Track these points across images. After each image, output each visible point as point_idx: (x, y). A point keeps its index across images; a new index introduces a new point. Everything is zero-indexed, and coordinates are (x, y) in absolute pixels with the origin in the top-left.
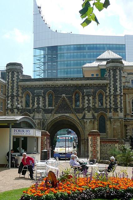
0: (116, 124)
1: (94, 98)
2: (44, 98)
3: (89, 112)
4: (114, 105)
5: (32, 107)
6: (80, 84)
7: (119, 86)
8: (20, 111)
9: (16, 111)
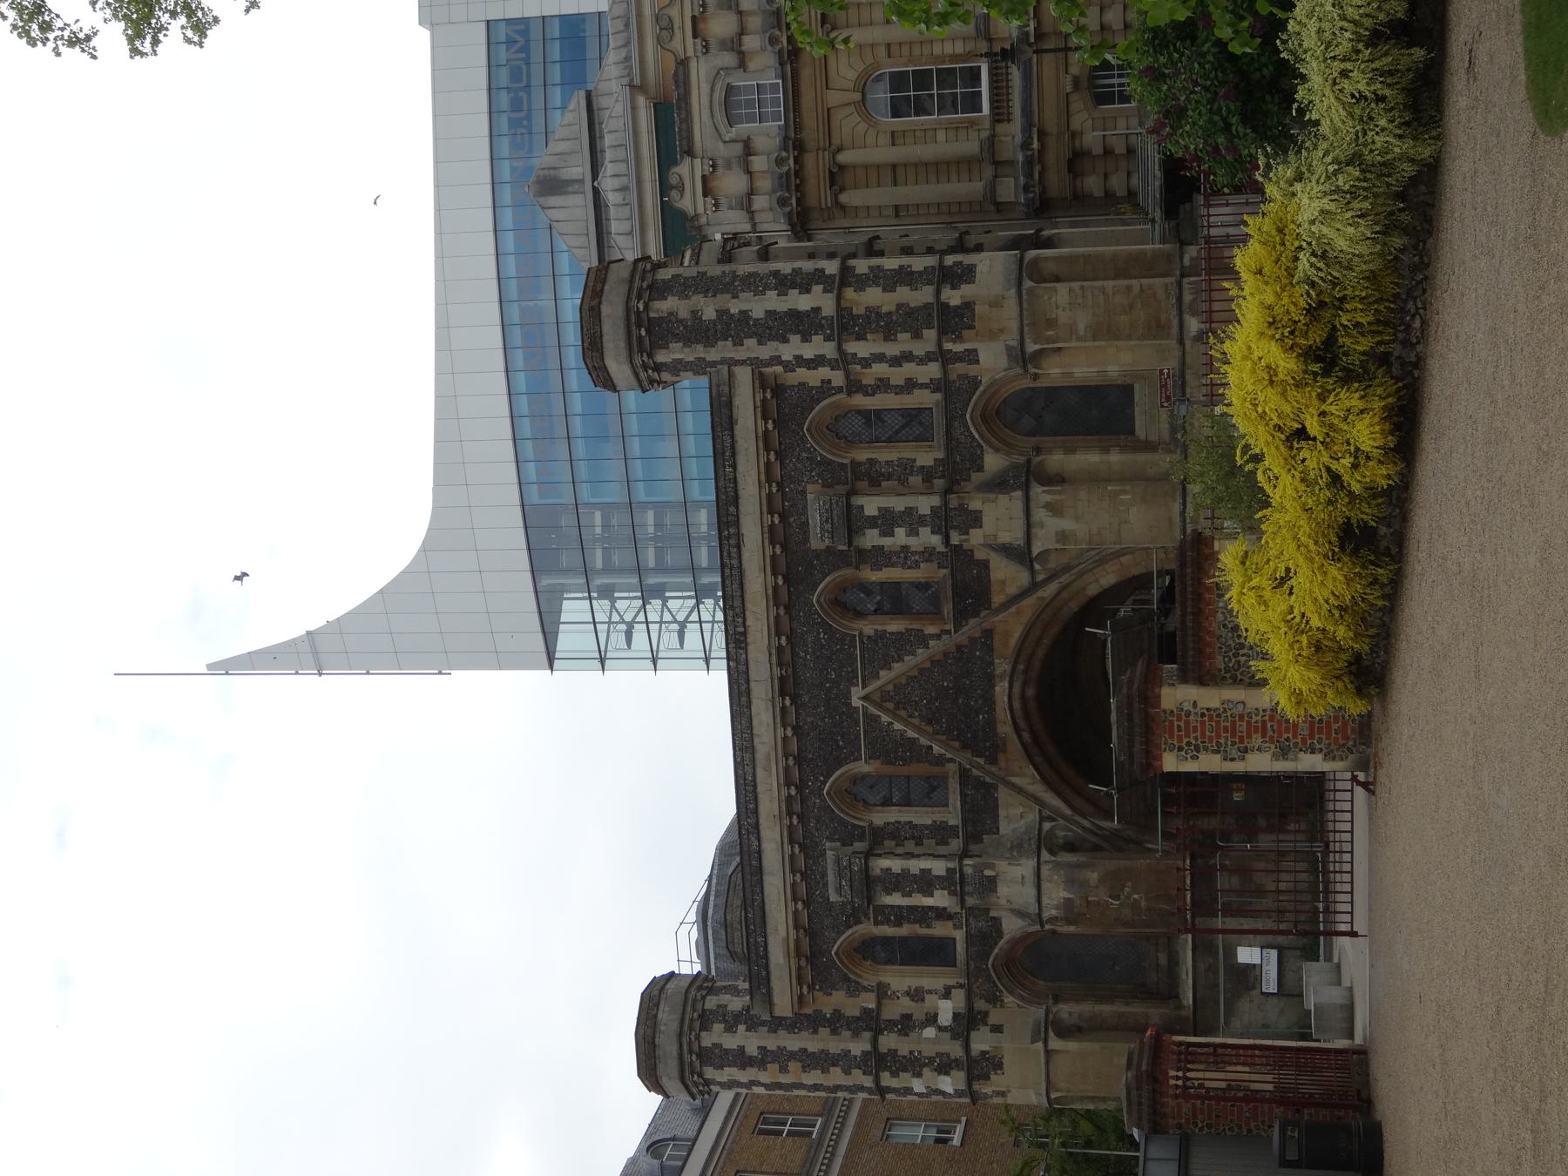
0: (1063, 317)
1: (874, 478)
2: (879, 839)
3: (976, 520)
4: (917, 335)
5: (950, 924)
6: (770, 578)
7: (773, 301)
8: (980, 1005)
9: (981, 1042)
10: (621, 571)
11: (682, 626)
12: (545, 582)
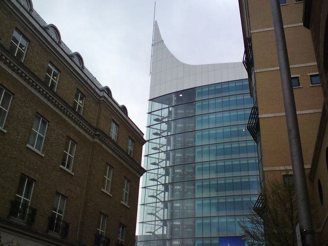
10: (174, 162)
11: (155, 197)
12: (173, 95)
